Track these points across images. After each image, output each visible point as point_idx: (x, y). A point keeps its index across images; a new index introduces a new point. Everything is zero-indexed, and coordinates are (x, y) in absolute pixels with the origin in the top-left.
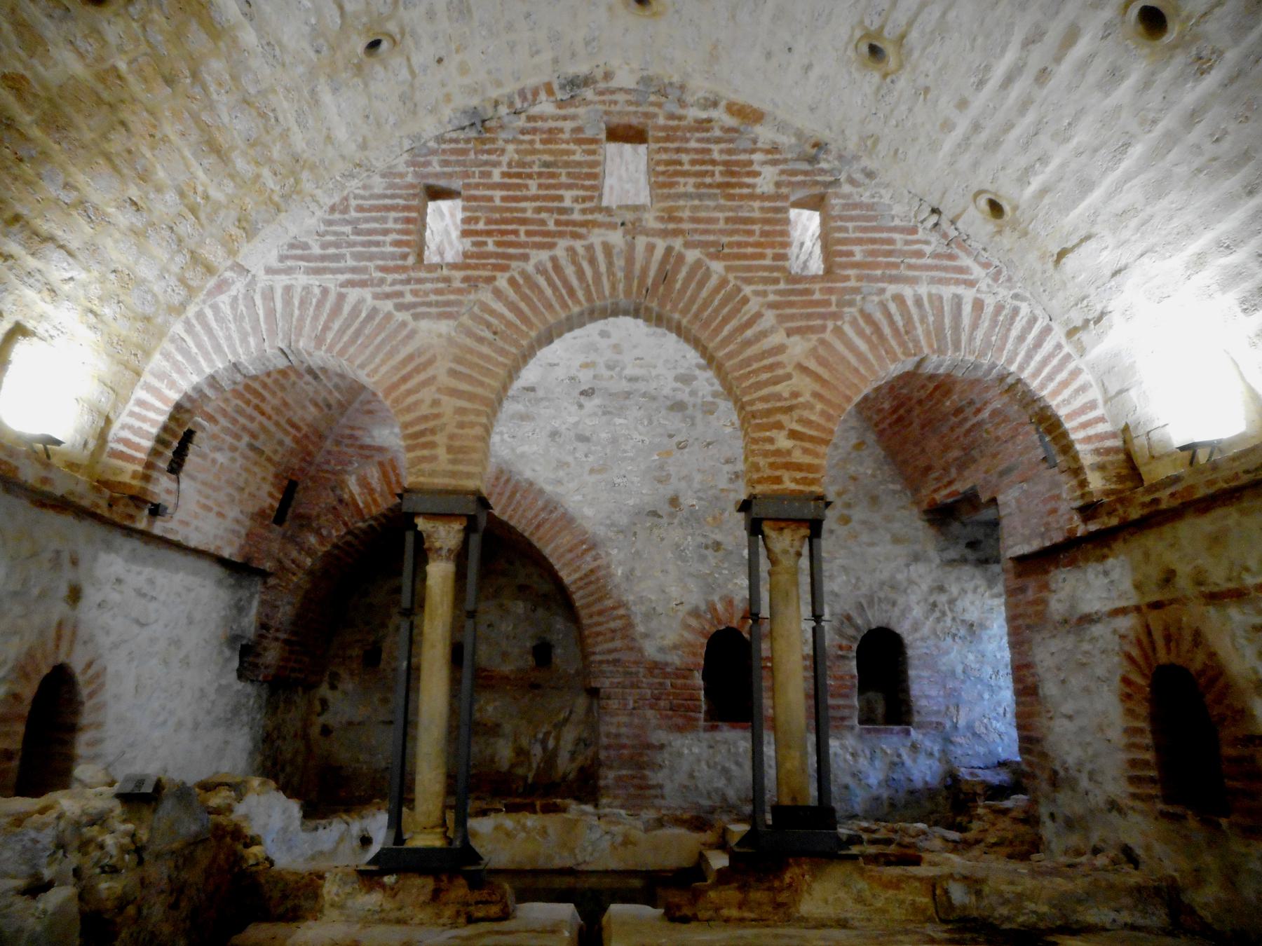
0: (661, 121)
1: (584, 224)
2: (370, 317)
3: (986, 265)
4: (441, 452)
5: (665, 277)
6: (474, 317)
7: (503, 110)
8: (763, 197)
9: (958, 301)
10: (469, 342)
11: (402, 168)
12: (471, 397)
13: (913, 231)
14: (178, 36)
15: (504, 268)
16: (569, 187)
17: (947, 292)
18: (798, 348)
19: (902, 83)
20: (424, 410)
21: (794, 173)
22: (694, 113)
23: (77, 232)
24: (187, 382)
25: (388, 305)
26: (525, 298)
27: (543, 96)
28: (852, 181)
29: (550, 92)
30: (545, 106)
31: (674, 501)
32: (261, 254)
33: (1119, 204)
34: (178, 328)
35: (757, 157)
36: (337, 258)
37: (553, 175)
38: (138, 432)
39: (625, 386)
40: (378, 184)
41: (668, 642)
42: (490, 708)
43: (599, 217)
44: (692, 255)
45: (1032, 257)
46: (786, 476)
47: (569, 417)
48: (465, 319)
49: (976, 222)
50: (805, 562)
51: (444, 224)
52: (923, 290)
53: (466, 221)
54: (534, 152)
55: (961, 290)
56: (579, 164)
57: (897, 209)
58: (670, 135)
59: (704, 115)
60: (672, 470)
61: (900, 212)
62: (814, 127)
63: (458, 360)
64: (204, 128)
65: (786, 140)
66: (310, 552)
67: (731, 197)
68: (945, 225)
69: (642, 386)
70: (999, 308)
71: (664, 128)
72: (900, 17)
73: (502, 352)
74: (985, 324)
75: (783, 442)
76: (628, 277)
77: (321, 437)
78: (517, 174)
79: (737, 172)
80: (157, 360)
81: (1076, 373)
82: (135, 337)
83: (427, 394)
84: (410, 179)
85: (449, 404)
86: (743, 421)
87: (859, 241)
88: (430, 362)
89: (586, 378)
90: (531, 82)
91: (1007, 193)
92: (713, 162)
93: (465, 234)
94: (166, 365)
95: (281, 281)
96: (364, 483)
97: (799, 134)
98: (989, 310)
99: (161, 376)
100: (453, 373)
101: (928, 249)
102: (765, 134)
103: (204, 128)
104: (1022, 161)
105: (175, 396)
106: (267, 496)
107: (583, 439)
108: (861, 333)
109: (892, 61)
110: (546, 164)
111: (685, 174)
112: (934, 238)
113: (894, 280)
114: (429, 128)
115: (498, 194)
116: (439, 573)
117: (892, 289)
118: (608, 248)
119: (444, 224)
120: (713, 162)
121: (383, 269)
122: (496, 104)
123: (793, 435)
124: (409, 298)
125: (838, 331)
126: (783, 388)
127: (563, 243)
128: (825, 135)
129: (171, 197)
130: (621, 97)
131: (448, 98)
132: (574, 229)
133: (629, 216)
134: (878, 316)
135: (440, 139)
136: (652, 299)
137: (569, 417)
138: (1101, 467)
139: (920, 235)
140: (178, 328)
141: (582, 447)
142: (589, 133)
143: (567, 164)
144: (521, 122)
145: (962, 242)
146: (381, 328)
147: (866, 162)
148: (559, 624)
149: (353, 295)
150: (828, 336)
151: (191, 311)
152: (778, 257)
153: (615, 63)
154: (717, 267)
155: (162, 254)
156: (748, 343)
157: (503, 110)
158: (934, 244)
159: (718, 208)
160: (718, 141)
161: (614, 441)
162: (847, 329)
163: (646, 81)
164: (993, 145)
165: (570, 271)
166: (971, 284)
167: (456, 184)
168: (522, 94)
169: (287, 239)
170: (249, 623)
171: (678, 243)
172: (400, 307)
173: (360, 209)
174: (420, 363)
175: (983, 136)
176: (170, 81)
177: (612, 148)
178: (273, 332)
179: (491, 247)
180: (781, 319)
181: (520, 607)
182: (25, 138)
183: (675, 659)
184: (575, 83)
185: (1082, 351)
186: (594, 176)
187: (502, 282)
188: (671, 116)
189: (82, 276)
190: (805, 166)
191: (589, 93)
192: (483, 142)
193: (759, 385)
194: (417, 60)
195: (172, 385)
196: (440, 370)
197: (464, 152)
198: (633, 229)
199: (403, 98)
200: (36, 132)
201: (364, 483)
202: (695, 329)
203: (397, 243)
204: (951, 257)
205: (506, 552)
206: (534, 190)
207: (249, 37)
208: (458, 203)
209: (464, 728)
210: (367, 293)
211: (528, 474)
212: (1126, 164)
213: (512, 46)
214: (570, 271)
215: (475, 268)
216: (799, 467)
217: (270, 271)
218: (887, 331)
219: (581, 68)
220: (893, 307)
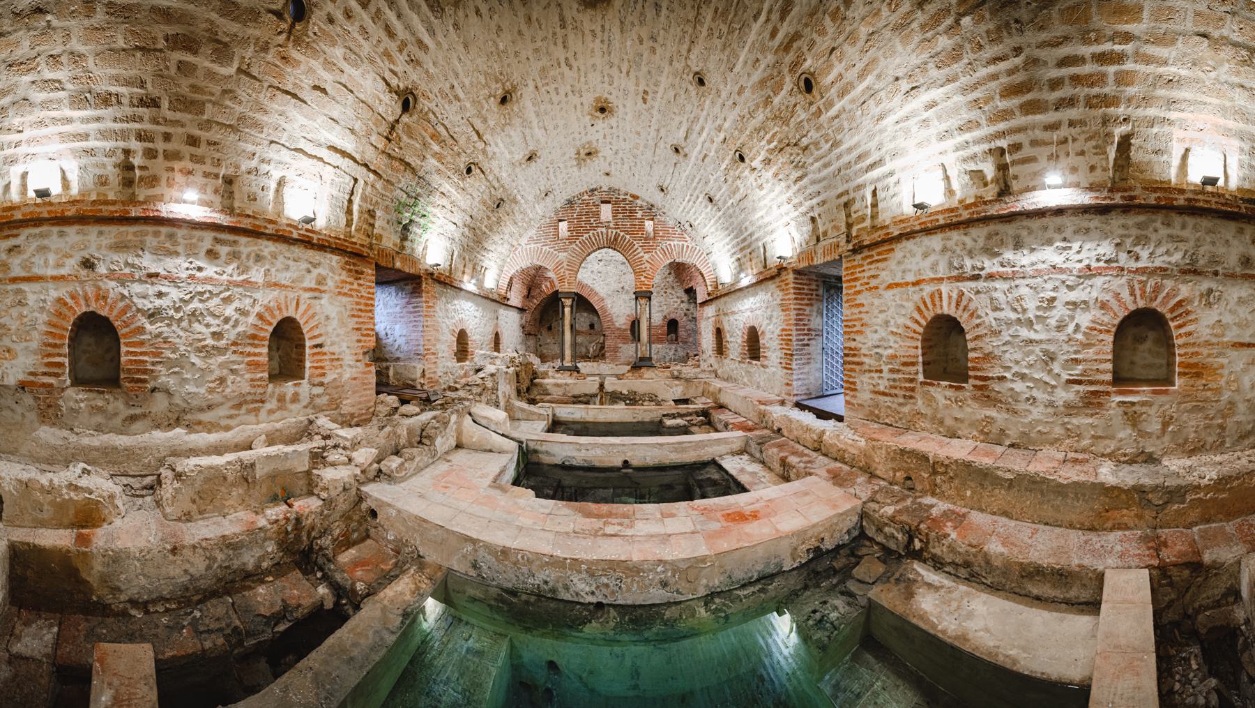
5: (616, 239)
18: (646, 256)
24: (512, 272)
30: (586, 197)
32: (523, 241)
42: (580, 339)
51: (563, 226)
58: (616, 203)
61: (671, 223)
62: (651, 201)
78: (580, 215)
79: (632, 212)
102: (639, 202)
106: (525, 292)
114: (559, 205)
116: (567, 310)
119: (563, 226)
132: (594, 228)
136: (613, 244)
184: (593, 190)
198: (608, 227)
205: (582, 303)
209: (574, 345)
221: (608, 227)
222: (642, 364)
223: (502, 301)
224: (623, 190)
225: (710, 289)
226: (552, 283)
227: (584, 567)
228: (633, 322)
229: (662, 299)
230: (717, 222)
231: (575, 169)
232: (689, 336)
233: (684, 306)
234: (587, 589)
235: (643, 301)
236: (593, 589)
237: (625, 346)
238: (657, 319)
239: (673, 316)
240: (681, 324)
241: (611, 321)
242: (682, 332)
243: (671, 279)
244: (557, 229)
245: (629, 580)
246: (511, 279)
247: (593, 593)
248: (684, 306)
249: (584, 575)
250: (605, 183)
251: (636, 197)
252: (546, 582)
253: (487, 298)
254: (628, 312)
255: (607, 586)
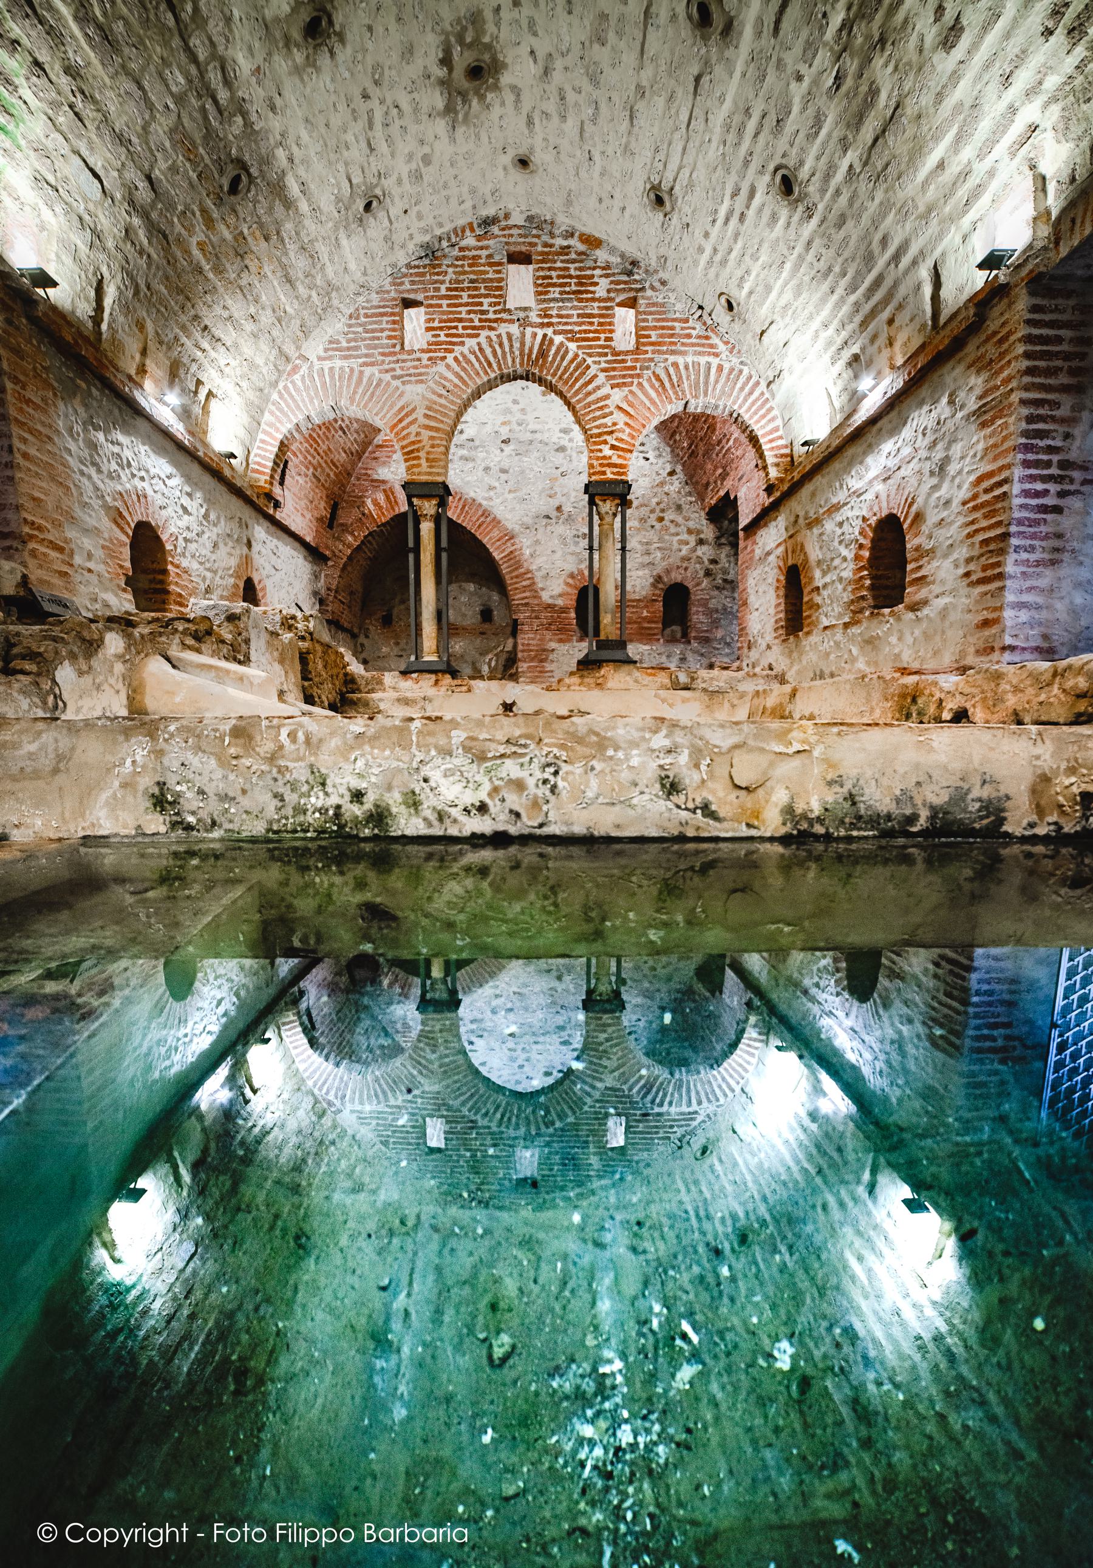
0: (540, 248)
1: (496, 321)
2: (378, 385)
3: (727, 343)
4: (423, 462)
5: (543, 354)
6: (437, 383)
7: (445, 244)
8: (599, 300)
9: (709, 365)
10: (435, 398)
11: (387, 287)
12: (437, 430)
13: (687, 321)
14: (270, 210)
15: (451, 351)
16: (486, 296)
17: (703, 360)
18: (617, 396)
19: (675, 221)
20: (412, 438)
21: (618, 283)
22: (559, 242)
23: (228, 335)
24: (285, 428)
25: (387, 377)
26: (464, 369)
27: (468, 233)
28: (653, 288)
29: (472, 230)
30: (470, 241)
31: (559, 509)
32: (314, 348)
33: (782, 302)
34: (275, 396)
35: (598, 272)
36: (357, 348)
37: (476, 289)
38: (263, 457)
39: (529, 436)
40: (375, 298)
41: (556, 592)
43: (504, 316)
44: (558, 339)
45: (749, 336)
46: (608, 470)
47: (496, 457)
48: (431, 384)
49: (721, 316)
50: (618, 518)
51: (415, 321)
52: (689, 359)
53: (428, 321)
54: (465, 273)
55: (711, 359)
56: (491, 280)
57: (679, 307)
58: (545, 258)
59: (565, 243)
60: (557, 489)
61: (680, 308)
62: (630, 249)
63: (429, 408)
64: (284, 267)
65: (615, 260)
66: (349, 546)
67: (580, 300)
68: (705, 317)
69: (538, 436)
70: (732, 370)
71: (542, 253)
72: (669, 175)
73: (452, 402)
74: (723, 380)
75: (607, 452)
76: (522, 354)
77: (349, 475)
79: (585, 282)
80: (267, 415)
81: (771, 409)
82: (257, 401)
83: (413, 429)
84: (393, 294)
85: (426, 434)
86: (587, 440)
87: (655, 328)
88: (414, 410)
89: (505, 433)
90: (461, 222)
91: (740, 296)
92: (570, 277)
93: (428, 329)
94: (272, 419)
95: (327, 364)
96: (376, 503)
97: (623, 256)
98: (726, 371)
99: (271, 425)
100: (426, 416)
101: (694, 333)
102: (602, 255)
103: (284, 267)
104: (739, 273)
105: (280, 437)
106: (324, 511)
107: (504, 471)
108: (652, 386)
109: (668, 204)
110: (472, 281)
111: (554, 285)
112: (698, 325)
113: (673, 352)
114: (401, 258)
115: (445, 302)
117: (672, 358)
118: (509, 336)
120: (570, 277)
121: (383, 354)
122: (440, 239)
123: (613, 447)
124: (399, 372)
125: (640, 384)
126: (608, 421)
127: (484, 333)
128: (639, 256)
129: (269, 312)
130: (515, 231)
131: (411, 237)
132: (490, 324)
133: (522, 315)
134: (663, 376)
135: (408, 266)
136: (534, 370)
137: (496, 457)
138: (777, 465)
139: (691, 324)
140: (275, 396)
141: (504, 477)
142: (497, 258)
143: (484, 281)
144: (456, 252)
145: (714, 328)
146: (385, 390)
147: (662, 275)
148: (496, 597)
149: (368, 371)
150: (634, 388)
151: (281, 385)
152: (608, 339)
153: (511, 206)
154: (572, 346)
155: (265, 348)
156: (589, 394)
157: (445, 244)
158: (699, 329)
159: (573, 308)
160: (574, 261)
161: (522, 472)
162: (646, 384)
163: (530, 219)
164: (724, 262)
165: (488, 351)
166: (716, 355)
167: (420, 297)
168: (455, 230)
169: (327, 338)
170: (321, 584)
171: (549, 331)
172: (394, 377)
173: (366, 316)
174: (406, 413)
175: (718, 258)
176: (267, 238)
177: (512, 268)
178: (326, 396)
179: (443, 338)
180: (609, 378)
181: (471, 587)
182: (207, 279)
183: (560, 602)
184: (488, 222)
185: (773, 396)
186: (500, 288)
187: (450, 358)
188: (546, 245)
189: (233, 363)
190: (625, 278)
191: (495, 230)
192: (434, 267)
193: (595, 419)
194: (393, 212)
195: (277, 430)
196: (419, 414)
197: (423, 274)
198: (524, 323)
199: (386, 239)
200: (211, 275)
201: (376, 503)
202: (560, 385)
203: (389, 337)
204: (707, 338)
206: (465, 300)
207: (304, 206)
208: (422, 309)
210: (375, 370)
211: (472, 495)
212: (785, 274)
213: (448, 198)
214: (488, 351)
215: (436, 350)
216: (615, 465)
217: (320, 358)
218: (667, 385)
219: (490, 211)
220: (671, 370)
221: (524, 323)
222: (605, 654)
223: (260, 504)
224: (563, 222)
225: (773, 473)
226: (389, 494)
227: (458, 736)
228: (583, 593)
229: (652, 535)
230: (797, 267)
231: (441, 126)
232: (715, 624)
233: (705, 552)
234: (470, 798)
235: (607, 507)
236: (483, 795)
237: (563, 648)
238: (640, 582)
239: (676, 577)
240: (697, 595)
241: (532, 587)
242: (698, 617)
243: (675, 485)
244: (399, 324)
245: (577, 769)
246: (283, 447)
247: (482, 808)
248: (705, 552)
249: (460, 760)
250: (516, 198)
251: (593, 242)
252: (358, 796)
253: (216, 474)
254: (571, 566)
255: (519, 785)
